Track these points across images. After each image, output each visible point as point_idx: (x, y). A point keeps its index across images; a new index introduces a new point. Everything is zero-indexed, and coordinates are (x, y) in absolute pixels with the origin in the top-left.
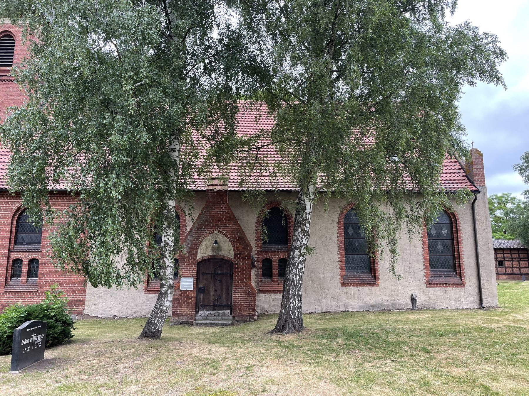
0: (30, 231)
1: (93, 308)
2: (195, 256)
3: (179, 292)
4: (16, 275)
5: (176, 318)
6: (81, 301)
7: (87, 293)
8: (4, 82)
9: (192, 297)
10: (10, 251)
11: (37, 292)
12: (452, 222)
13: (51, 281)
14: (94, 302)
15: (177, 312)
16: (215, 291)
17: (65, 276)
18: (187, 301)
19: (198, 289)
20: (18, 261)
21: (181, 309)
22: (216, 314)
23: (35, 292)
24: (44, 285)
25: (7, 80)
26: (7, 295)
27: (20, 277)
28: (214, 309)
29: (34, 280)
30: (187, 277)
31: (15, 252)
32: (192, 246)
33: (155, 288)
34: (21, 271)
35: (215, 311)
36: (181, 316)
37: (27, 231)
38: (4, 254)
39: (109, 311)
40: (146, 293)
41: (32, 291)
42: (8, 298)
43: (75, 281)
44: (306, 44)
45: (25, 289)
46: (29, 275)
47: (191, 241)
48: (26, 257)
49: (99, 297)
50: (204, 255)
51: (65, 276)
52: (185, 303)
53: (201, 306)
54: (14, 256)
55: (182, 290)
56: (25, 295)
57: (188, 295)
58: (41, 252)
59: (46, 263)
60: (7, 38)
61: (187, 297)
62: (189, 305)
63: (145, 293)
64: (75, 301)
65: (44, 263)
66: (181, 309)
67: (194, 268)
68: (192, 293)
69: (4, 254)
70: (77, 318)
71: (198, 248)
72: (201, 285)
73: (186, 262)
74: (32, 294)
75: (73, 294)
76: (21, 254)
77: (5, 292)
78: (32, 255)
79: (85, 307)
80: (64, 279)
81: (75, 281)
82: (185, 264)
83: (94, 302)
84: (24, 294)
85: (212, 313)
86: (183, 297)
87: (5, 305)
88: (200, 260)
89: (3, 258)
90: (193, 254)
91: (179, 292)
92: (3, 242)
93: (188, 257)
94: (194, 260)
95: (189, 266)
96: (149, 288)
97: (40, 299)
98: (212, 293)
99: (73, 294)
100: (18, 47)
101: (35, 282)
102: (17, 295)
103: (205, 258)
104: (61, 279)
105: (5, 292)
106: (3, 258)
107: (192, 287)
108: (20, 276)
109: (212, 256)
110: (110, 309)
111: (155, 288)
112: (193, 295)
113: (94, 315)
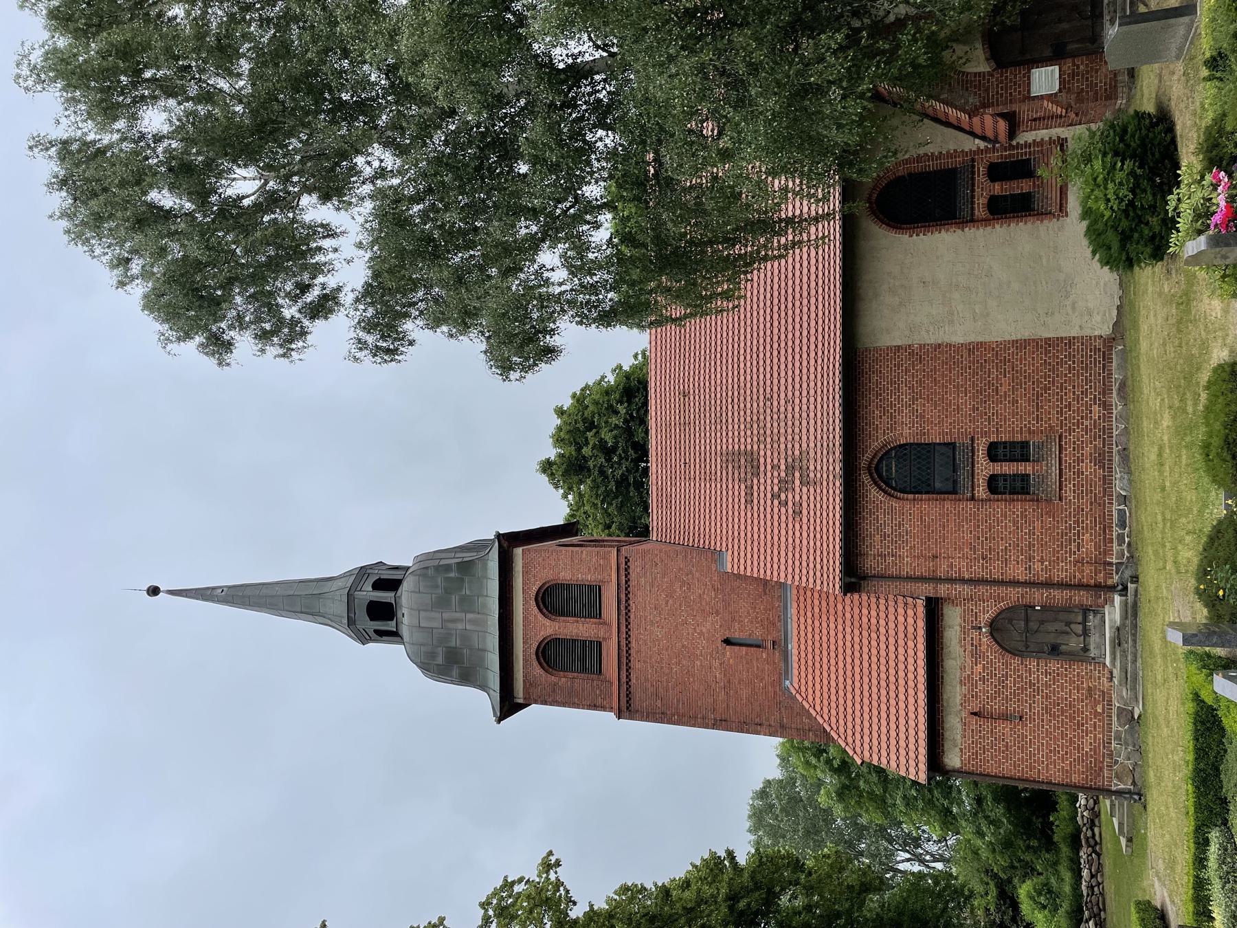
0: (929, 468)
1: (1098, 318)
2: (984, 77)
3: (1063, 94)
4: (1023, 488)
5: (1120, 90)
6: (1082, 344)
7: (1064, 335)
8: (630, 596)
9: (1074, 64)
10: (973, 498)
11: (1060, 437)
12: (938, 493)
13: (1037, 411)
14: (1086, 318)
15: (1106, 89)
16: (1060, 21)
17: (1025, 384)
18: (1083, 75)
19: (1056, 55)
20: (993, 484)
21: (1101, 82)
22: (1112, 9)
23: (1060, 464)
24: (1046, 423)
25: (626, 589)
26: (1069, 493)
27: (1028, 475)
28: (1101, 16)
29: (1034, 450)
30: (1029, 84)
31: (973, 489)
32: (963, 86)
33: (1054, 197)
34: (1014, 475)
35: (1105, 12)
36: (1116, 81)
37: (928, 474)
38: (978, 509)
39: (1105, 285)
40: (1067, 212)
41: (1060, 446)
42: (1074, 492)
43: (1038, 363)
44: (572, 211)
45: (1055, 462)
46: (1025, 458)
47: (950, 91)
48: (984, 468)
49: (1074, 308)
50: (982, 57)
51: (1025, 384)
52: (1087, 78)
53: (1094, 43)
54: (981, 491)
55: (1057, 88)
56: (1067, 459)
57: (1069, 75)
58: (972, 439)
59: (997, 424)
60: (548, 600)
61: (1073, 75)
62: (1092, 68)
63: (1067, 216)
64: (1082, 357)
65: (997, 429)
66: (1101, 82)
67: (1011, 73)
68: (1065, 68)
69: (978, 509)
70: (1120, 348)
71: (968, 73)
72: (1048, 53)
73: (997, 92)
74: (1066, 444)
75: (1066, 363)
76: (978, 480)
77: (1060, 499)
78: (981, 456)
79: (1096, 333)
80: (1033, 384)
81: (1038, 363)
82: (1002, 94)
83: (1086, 318)
84: (1066, 461)
85: (1108, 18)
86: (1073, 84)
87: (1091, 497)
88: (993, 64)
89: (986, 510)
90: (980, 81)
91: (1063, 94)
92: (951, 512)
93: (987, 90)
94: (992, 76)
95: (1007, 84)
96: (1054, 209)
97: (1078, 428)
98: (1065, 26)
99: (1066, 363)
100: (565, 575)
101: (1040, 447)
102: (1068, 474)
103: (988, 55)
104: (1034, 389)
105: (1060, 499)
106: (986, 510)
107: (1050, 68)
108: (1025, 478)
109: (983, 41)
110: (1102, 284)
111: (1054, 197)
112: (1069, 63)
113: (1115, 312)
